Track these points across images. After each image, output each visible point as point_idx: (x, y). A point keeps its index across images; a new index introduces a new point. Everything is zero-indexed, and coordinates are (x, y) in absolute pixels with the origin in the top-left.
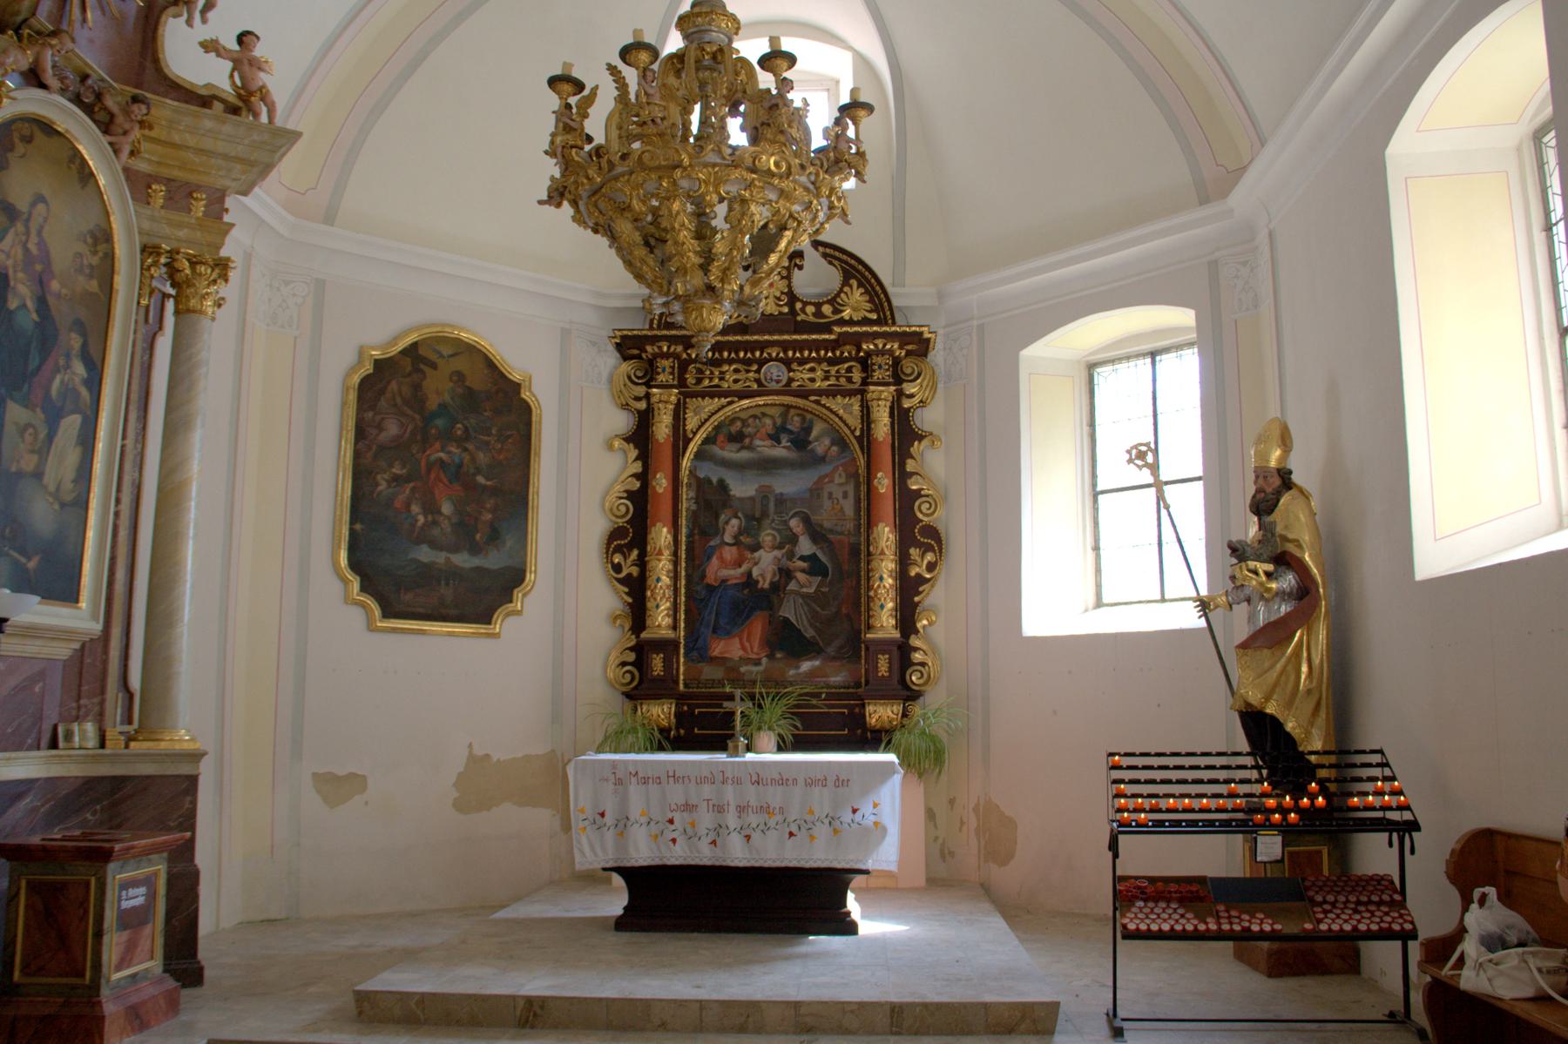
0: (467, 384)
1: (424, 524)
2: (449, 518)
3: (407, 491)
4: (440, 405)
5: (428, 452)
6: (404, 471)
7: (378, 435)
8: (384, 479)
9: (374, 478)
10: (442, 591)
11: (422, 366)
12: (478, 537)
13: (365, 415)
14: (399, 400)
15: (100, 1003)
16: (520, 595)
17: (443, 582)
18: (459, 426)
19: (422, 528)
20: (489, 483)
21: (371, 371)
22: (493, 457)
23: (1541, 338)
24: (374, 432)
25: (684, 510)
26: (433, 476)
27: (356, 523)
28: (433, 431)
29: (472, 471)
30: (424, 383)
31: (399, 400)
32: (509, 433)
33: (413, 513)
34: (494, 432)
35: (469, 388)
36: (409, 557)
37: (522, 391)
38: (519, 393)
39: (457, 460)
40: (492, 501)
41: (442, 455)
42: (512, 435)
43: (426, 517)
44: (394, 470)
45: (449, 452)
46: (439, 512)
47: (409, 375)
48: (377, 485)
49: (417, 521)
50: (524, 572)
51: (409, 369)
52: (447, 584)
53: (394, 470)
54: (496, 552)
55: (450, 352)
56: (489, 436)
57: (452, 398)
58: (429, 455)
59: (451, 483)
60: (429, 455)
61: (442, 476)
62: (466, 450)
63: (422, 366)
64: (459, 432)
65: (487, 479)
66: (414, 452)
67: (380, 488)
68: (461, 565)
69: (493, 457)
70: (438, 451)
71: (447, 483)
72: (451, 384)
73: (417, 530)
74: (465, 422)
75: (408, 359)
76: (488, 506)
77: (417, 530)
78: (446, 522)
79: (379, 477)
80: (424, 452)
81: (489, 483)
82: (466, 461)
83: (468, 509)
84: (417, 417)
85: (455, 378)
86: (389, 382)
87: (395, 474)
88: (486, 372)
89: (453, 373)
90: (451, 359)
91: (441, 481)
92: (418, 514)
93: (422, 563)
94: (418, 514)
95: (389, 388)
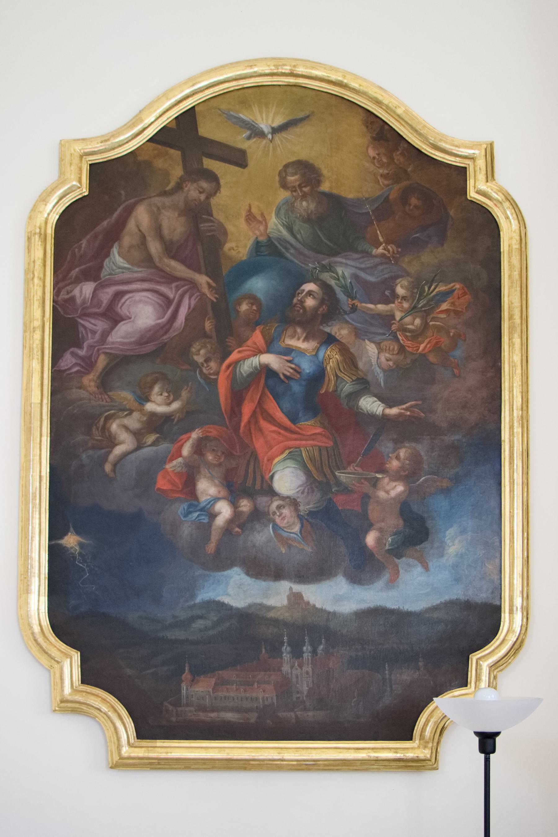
0: (325, 187)
1: (231, 522)
2: (293, 502)
3: (186, 450)
4: (257, 244)
5: (234, 356)
6: (176, 405)
7: (106, 334)
8: (126, 428)
9: (105, 429)
10: (286, 668)
11: (209, 164)
12: (371, 539)
13: (76, 292)
14: (155, 247)
15: (65, 547)
16: (485, 665)
17: (286, 649)
18: (310, 287)
19: (227, 530)
20: (394, 411)
21: (86, 194)
22: (402, 349)
23: (236, 79)
24: (100, 325)
25: (306, 70)
26: (247, 409)
27: (64, 533)
28: (244, 307)
29: (348, 388)
30: (214, 201)
31: (155, 247)
32: (442, 288)
33: (203, 499)
34: (400, 291)
35: (329, 196)
36: (198, 600)
37: (470, 183)
38: (464, 191)
39: (307, 367)
40: (402, 453)
41: (269, 359)
42: (450, 292)
43: (234, 504)
44: (149, 407)
45: (288, 351)
46: (271, 493)
47: (179, 187)
48: (112, 442)
49: (213, 516)
50: (497, 610)
51: (177, 172)
52: (297, 653)
53: (149, 407)
54: (419, 569)
55: (278, 121)
56: (387, 301)
57: (290, 229)
58: (236, 363)
59: (294, 419)
60: (236, 363)
61: (272, 407)
62: (330, 340)
63: (209, 164)
64: (310, 302)
65: (389, 402)
66: (199, 359)
67: (118, 450)
68: (329, 608)
69: (402, 349)
70: (260, 352)
71: (285, 421)
72: (284, 195)
73: (215, 536)
74: (326, 276)
75: (176, 154)
76: (395, 464)
77: (215, 536)
78: (286, 511)
79: (114, 427)
80: (226, 354)
81: (394, 411)
82: (330, 366)
83: (343, 477)
84: (203, 280)
85: (292, 179)
86: (129, 211)
87: (153, 414)
88: (372, 153)
89: (286, 166)
90: (278, 138)
91: (271, 420)
92: (216, 499)
93: (231, 608)
94: (216, 499)
95: (131, 225)
